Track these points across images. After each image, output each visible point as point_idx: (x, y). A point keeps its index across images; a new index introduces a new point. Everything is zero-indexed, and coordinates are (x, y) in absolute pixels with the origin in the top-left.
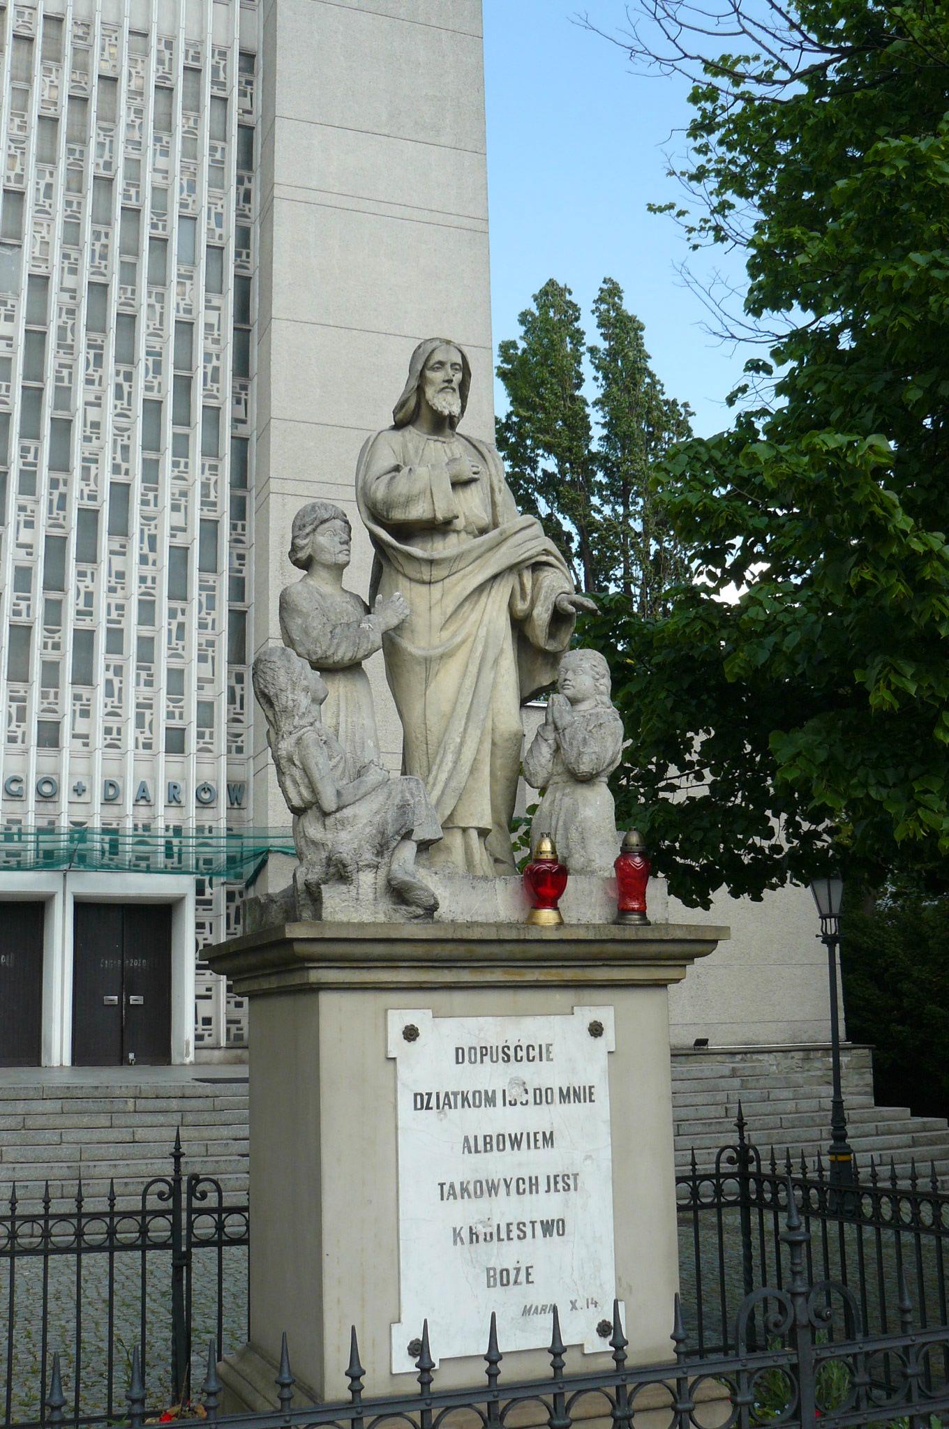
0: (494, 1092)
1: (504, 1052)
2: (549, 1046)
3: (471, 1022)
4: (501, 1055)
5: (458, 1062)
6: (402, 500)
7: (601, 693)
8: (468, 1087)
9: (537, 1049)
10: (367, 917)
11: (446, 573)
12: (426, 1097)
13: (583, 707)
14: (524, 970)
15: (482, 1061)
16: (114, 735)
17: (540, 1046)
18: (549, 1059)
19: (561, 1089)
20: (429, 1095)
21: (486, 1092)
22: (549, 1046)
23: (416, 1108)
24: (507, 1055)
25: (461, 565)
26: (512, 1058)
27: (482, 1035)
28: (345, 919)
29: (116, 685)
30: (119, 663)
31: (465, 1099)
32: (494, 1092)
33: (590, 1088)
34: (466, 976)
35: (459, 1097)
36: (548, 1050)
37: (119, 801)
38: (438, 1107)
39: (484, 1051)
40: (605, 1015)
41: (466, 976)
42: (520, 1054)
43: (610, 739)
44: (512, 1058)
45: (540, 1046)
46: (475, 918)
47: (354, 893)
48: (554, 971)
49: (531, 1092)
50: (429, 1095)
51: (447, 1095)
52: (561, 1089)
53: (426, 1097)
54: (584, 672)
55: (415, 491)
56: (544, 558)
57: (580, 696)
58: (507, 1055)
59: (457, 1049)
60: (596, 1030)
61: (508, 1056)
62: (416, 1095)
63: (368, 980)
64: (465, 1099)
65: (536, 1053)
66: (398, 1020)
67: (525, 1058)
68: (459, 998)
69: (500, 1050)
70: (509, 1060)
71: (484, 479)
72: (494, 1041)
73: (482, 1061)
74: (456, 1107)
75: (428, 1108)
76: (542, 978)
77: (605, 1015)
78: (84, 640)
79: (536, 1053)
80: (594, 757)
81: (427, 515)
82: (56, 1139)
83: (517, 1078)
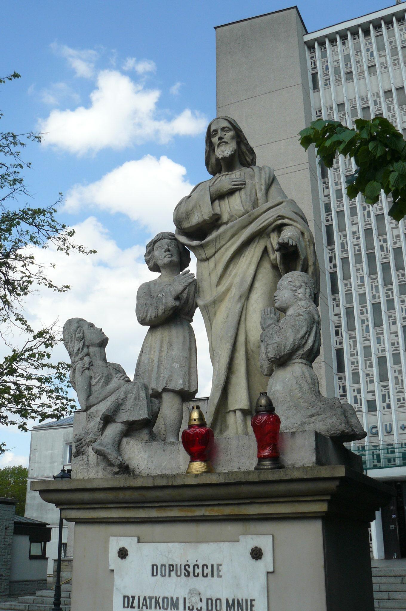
0: (177, 599)
1: (185, 569)
2: (219, 565)
3: (162, 546)
4: (183, 571)
5: (153, 575)
6: (184, 215)
7: (301, 300)
8: (160, 593)
9: (210, 568)
10: (93, 475)
11: (213, 251)
12: (131, 599)
13: (290, 312)
14: (193, 508)
15: (170, 575)
16: (402, 401)
17: (212, 566)
18: (219, 576)
19: (227, 600)
20: (133, 597)
21: (172, 598)
22: (219, 565)
23: (124, 607)
24: (188, 571)
25: (222, 243)
26: (191, 574)
27: (170, 556)
28: (82, 477)
29: (400, 378)
30: (399, 368)
31: (157, 602)
32: (177, 599)
33: (252, 601)
34: (154, 513)
35: (153, 601)
36: (218, 569)
37: (392, 434)
38: (139, 607)
39: (172, 568)
40: (265, 543)
41: (154, 513)
42: (197, 571)
43: (290, 330)
44: (191, 574)
45: (212, 566)
46: (164, 472)
47: (85, 460)
48: (216, 508)
49: (205, 601)
50: (133, 597)
51: (145, 599)
52: (227, 600)
53: (131, 599)
54: (285, 288)
55: (190, 208)
56: (280, 222)
57: (284, 306)
58: (188, 571)
59: (153, 566)
60: (257, 554)
61: (188, 572)
62: (125, 597)
63: (82, 517)
64: (157, 602)
65: (208, 571)
66: (115, 544)
67: (201, 575)
68: (158, 529)
69: (183, 567)
70: (189, 575)
71: (249, 187)
72: (178, 560)
73: (170, 575)
74: (151, 608)
75: (132, 607)
76: (207, 514)
77: (265, 543)
78: (382, 361)
79: (208, 571)
80: (275, 345)
81: (201, 220)
82: (386, 597)
83: (195, 589)
